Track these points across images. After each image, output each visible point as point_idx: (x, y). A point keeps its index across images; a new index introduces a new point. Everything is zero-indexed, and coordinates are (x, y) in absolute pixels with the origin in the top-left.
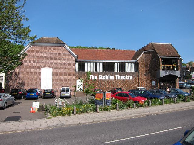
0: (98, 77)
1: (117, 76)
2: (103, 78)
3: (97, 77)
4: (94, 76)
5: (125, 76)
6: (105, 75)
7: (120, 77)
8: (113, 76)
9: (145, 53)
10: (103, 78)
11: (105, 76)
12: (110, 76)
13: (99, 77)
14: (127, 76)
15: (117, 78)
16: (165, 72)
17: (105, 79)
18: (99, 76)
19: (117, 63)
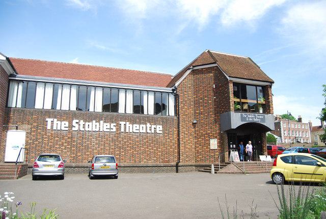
0: (71, 126)
1: (125, 123)
2: (84, 127)
3: (67, 123)
4: (59, 122)
5: (144, 126)
7: (131, 125)
11: (90, 124)
12: (105, 124)
13: (74, 124)
14: (148, 125)
15: (122, 130)
16: (242, 115)
17: (90, 129)
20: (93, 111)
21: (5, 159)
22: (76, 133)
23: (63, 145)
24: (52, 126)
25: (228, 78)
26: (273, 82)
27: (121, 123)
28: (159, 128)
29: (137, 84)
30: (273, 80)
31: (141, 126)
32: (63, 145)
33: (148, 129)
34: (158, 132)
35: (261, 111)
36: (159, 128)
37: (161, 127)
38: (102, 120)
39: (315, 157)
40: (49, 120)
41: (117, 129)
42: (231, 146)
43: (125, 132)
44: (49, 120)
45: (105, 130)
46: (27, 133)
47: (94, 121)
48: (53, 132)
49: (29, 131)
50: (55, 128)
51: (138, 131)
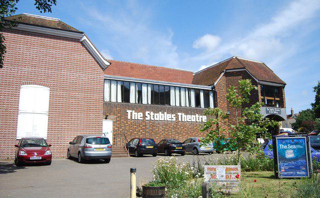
0: (145, 116)
1: (181, 114)
2: (154, 117)
3: (142, 114)
4: (136, 113)
5: (194, 116)
6: (158, 112)
7: (185, 116)
8: (173, 115)
9: (227, 75)
10: (154, 117)
11: (158, 114)
12: (168, 115)
13: (147, 115)
14: (197, 115)
15: (180, 120)
16: (266, 109)
17: (158, 119)
18: (147, 113)
19: (147, 84)
20: (146, 103)
21: (18, 135)
22: (148, 122)
23: (139, 132)
24: (131, 117)
25: (257, 81)
26: (285, 84)
27: (128, 111)
29: (171, 81)
31: (193, 116)
32: (139, 132)
33: (197, 118)
34: (204, 121)
35: (278, 106)
38: (165, 111)
40: (129, 112)
41: (176, 118)
43: (182, 121)
44: (129, 112)
45: (168, 120)
46: (114, 122)
47: (160, 113)
48: (132, 121)
49: (115, 120)
50: (133, 118)
51: (190, 121)
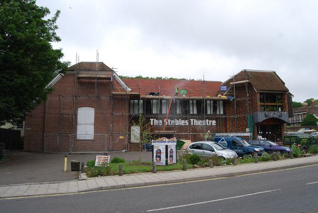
15: (192, 124)
24: (153, 123)
28: (214, 122)
30: (48, 7)
33: (169, 123)
35: (280, 110)
36: (214, 122)
37: (215, 121)
39: (294, 134)
40: (152, 120)
42: (260, 133)
44: (152, 120)
